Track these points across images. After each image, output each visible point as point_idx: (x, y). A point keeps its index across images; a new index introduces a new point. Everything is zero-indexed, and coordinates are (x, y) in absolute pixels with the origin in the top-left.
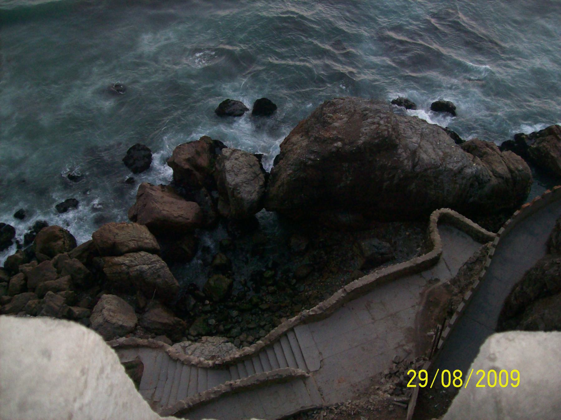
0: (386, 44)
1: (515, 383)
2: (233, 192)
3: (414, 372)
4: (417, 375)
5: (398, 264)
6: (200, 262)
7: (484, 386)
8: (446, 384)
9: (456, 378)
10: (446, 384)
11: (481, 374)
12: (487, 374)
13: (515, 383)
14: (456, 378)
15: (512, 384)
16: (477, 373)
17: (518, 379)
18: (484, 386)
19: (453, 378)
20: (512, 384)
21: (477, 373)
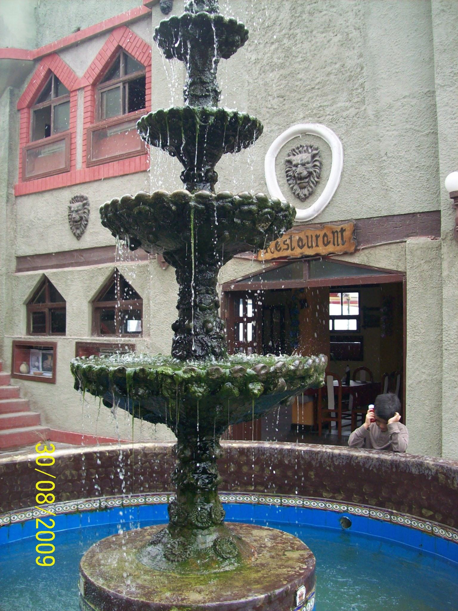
0: (285, 579)
1: (41, 561)
2: (358, 437)
3: (53, 526)
4: (48, 529)
5: (9, 47)
6: (111, 214)
7: (37, 527)
8: (40, 486)
9: (46, 497)
10: (40, 486)
11: (51, 524)
12: (51, 530)
13: (41, 561)
14: (46, 497)
15: (39, 558)
16: (51, 520)
17: (45, 564)
18: (37, 527)
19: (46, 493)
20: (39, 558)
21: (51, 520)
